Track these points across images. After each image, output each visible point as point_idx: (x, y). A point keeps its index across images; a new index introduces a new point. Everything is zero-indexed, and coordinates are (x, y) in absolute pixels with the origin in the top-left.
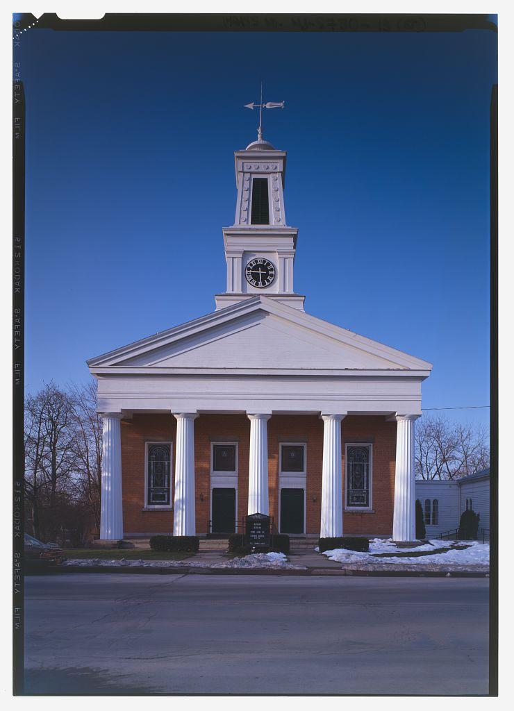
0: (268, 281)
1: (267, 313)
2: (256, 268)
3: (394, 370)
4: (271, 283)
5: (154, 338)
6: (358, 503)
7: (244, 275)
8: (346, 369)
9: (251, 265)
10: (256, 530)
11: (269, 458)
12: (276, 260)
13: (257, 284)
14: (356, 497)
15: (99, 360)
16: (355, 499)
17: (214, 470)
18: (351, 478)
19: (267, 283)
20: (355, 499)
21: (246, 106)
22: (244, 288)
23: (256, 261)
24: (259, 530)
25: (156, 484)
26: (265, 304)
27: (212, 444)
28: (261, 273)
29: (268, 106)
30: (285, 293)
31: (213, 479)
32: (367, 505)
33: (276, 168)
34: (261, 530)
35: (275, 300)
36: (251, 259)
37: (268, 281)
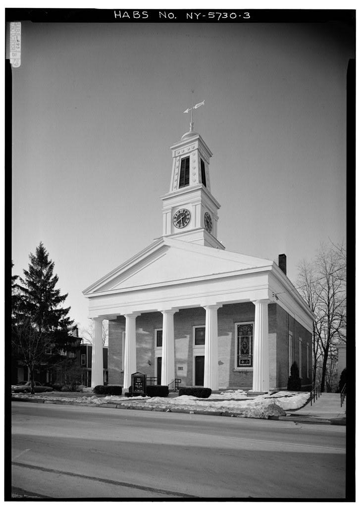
0: (186, 223)
1: (169, 247)
2: (179, 217)
3: (217, 274)
4: (188, 224)
5: (112, 274)
6: (245, 365)
7: (173, 222)
8: (213, 274)
9: (177, 215)
10: (138, 383)
11: (269, 333)
14: (244, 360)
16: (243, 362)
17: (157, 346)
18: (240, 347)
19: (185, 224)
20: (243, 362)
21: (185, 112)
22: (172, 230)
23: (179, 212)
24: (139, 382)
26: (167, 242)
27: (236, 325)
28: (182, 218)
30: (197, 227)
31: (194, 350)
32: (238, 366)
35: (172, 239)
37: (186, 223)
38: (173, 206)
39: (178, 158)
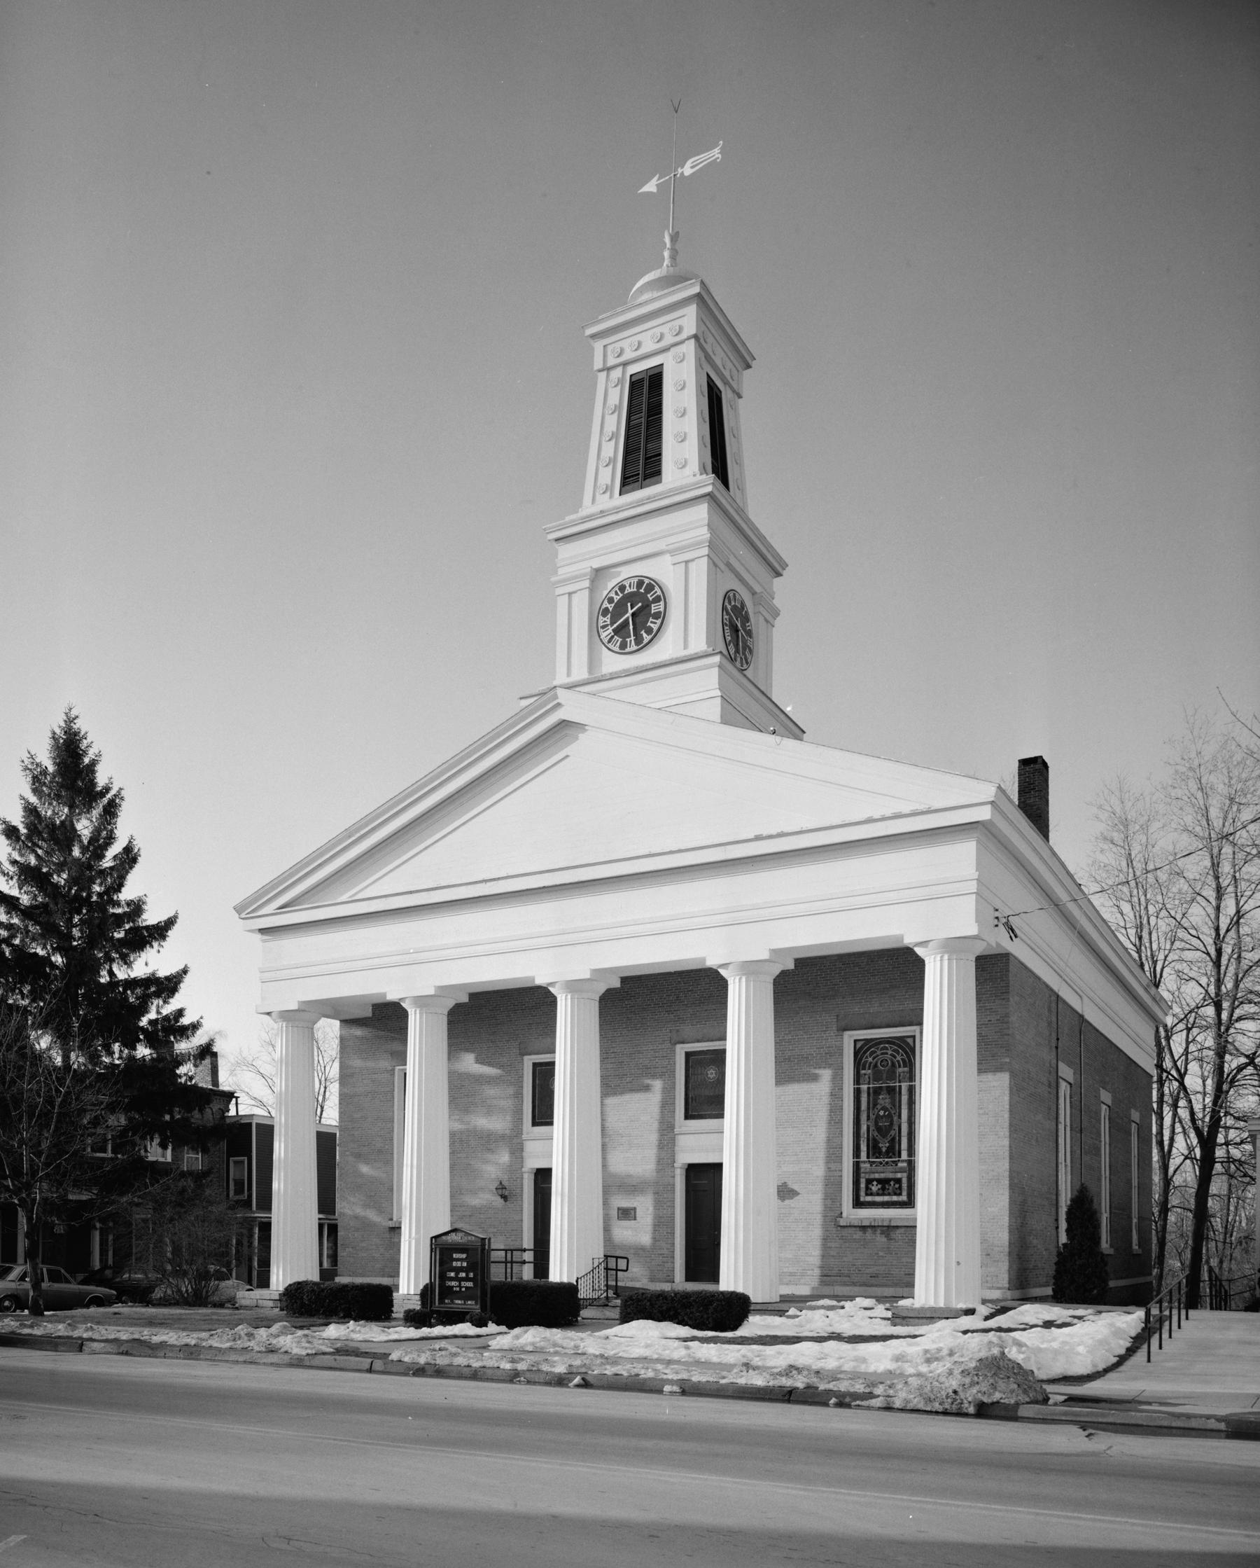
0: (649, 631)
1: (580, 727)
2: (620, 608)
4: (655, 635)
6: (886, 1198)
7: (594, 630)
8: (758, 838)
12: (664, 572)
13: (623, 646)
14: (879, 1181)
15: (256, 900)
16: (874, 1188)
19: (646, 638)
20: (874, 1188)
23: (622, 588)
25: (874, 1150)
29: (687, 170)
32: (858, 1203)
33: (681, 329)
34: (466, 1270)
36: (611, 584)
37: (649, 631)
38: (597, 564)
39: (617, 373)
